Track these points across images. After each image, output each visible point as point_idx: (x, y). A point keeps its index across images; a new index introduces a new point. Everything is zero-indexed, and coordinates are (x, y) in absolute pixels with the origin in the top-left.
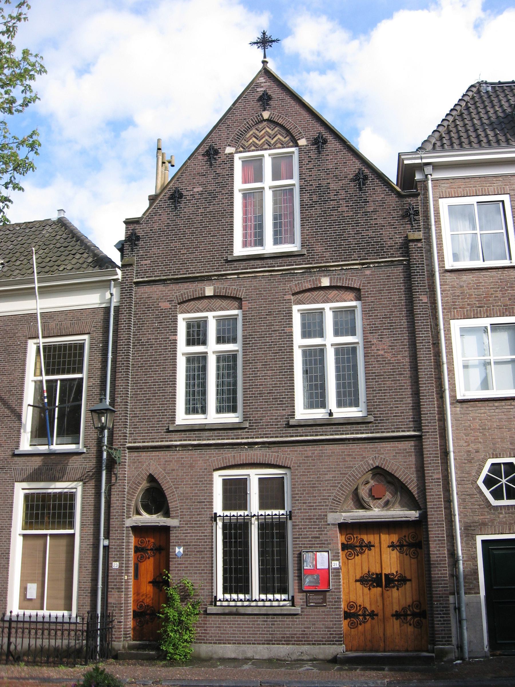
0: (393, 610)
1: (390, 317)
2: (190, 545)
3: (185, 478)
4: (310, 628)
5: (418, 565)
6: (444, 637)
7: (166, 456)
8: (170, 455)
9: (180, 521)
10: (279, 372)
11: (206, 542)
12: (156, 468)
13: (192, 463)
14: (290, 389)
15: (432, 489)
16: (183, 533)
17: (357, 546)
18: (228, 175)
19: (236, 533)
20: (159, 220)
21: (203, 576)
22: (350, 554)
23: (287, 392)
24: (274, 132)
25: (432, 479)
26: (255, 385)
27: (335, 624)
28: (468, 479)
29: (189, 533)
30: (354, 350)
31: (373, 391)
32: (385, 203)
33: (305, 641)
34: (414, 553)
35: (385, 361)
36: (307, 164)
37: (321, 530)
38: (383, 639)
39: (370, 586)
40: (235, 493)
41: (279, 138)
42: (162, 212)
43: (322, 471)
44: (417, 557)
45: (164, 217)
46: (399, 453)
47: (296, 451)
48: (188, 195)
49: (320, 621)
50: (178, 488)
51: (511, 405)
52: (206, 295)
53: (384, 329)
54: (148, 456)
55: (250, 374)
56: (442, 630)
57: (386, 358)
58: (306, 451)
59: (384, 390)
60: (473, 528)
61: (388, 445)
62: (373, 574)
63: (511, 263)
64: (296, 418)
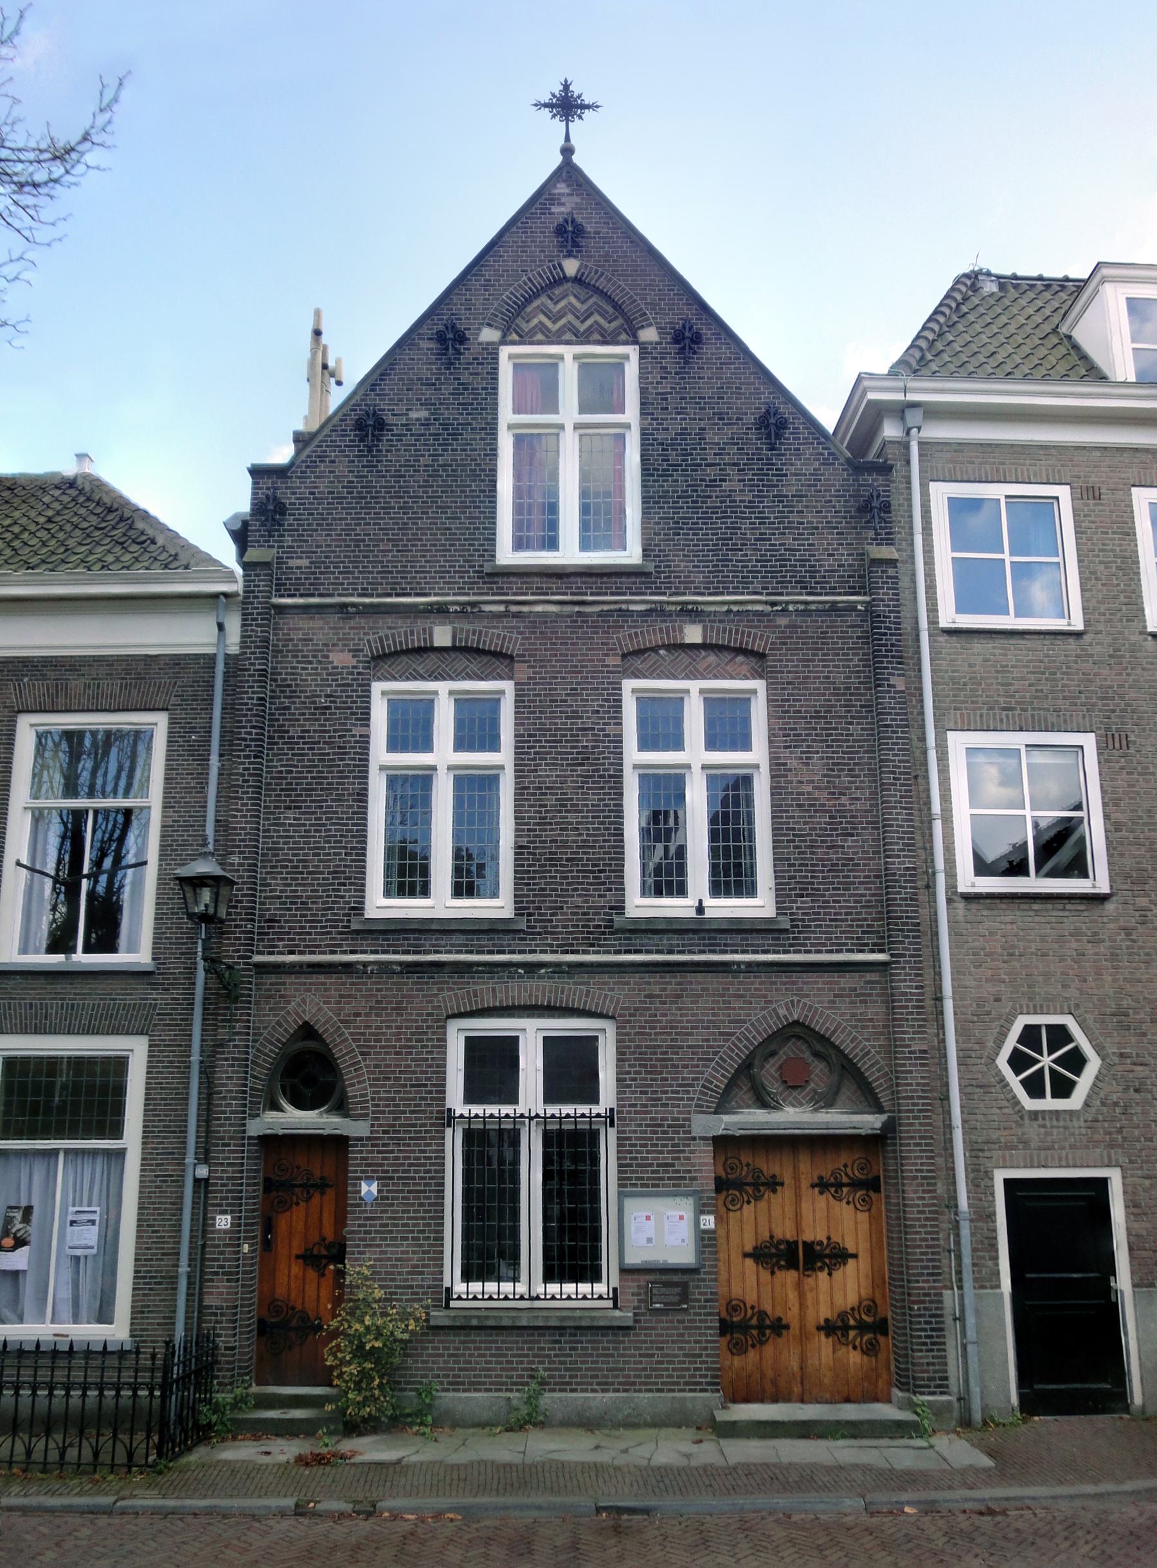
0: (818, 1317)
1: (826, 717)
2: (392, 1178)
3: (384, 1034)
4: (652, 1355)
5: (870, 1225)
6: (933, 1379)
7: (344, 984)
8: (352, 984)
9: (372, 1126)
10: (593, 817)
11: (428, 1171)
12: (320, 1009)
13: (401, 1002)
14: (615, 853)
15: (911, 1072)
16: (379, 1152)
17: (747, 1184)
18: (486, 389)
19: (491, 1151)
20: (330, 472)
21: (421, 1245)
22: (733, 1200)
23: (610, 859)
24: (585, 307)
25: (910, 1052)
26: (540, 842)
27: (706, 1349)
28: (975, 1056)
29: (392, 1152)
30: (747, 780)
31: (789, 865)
32: (820, 480)
33: (641, 1383)
34: (864, 1200)
35: (814, 805)
36: (658, 383)
37: (676, 1151)
38: (799, 1380)
39: (773, 1267)
40: (492, 1067)
41: (596, 322)
42: (336, 456)
43: (682, 1028)
44: (869, 1210)
45: (342, 467)
46: (841, 996)
47: (628, 983)
48: (397, 425)
49: (673, 1342)
50: (369, 1054)
51: (1064, 910)
52: (436, 645)
53: (814, 741)
54: (300, 984)
55: (529, 818)
56: (928, 1364)
57: (816, 799)
58: (649, 983)
59: (812, 865)
60: (987, 1154)
61: (820, 980)
62: (780, 1242)
63: (1069, 625)
64: (627, 915)
